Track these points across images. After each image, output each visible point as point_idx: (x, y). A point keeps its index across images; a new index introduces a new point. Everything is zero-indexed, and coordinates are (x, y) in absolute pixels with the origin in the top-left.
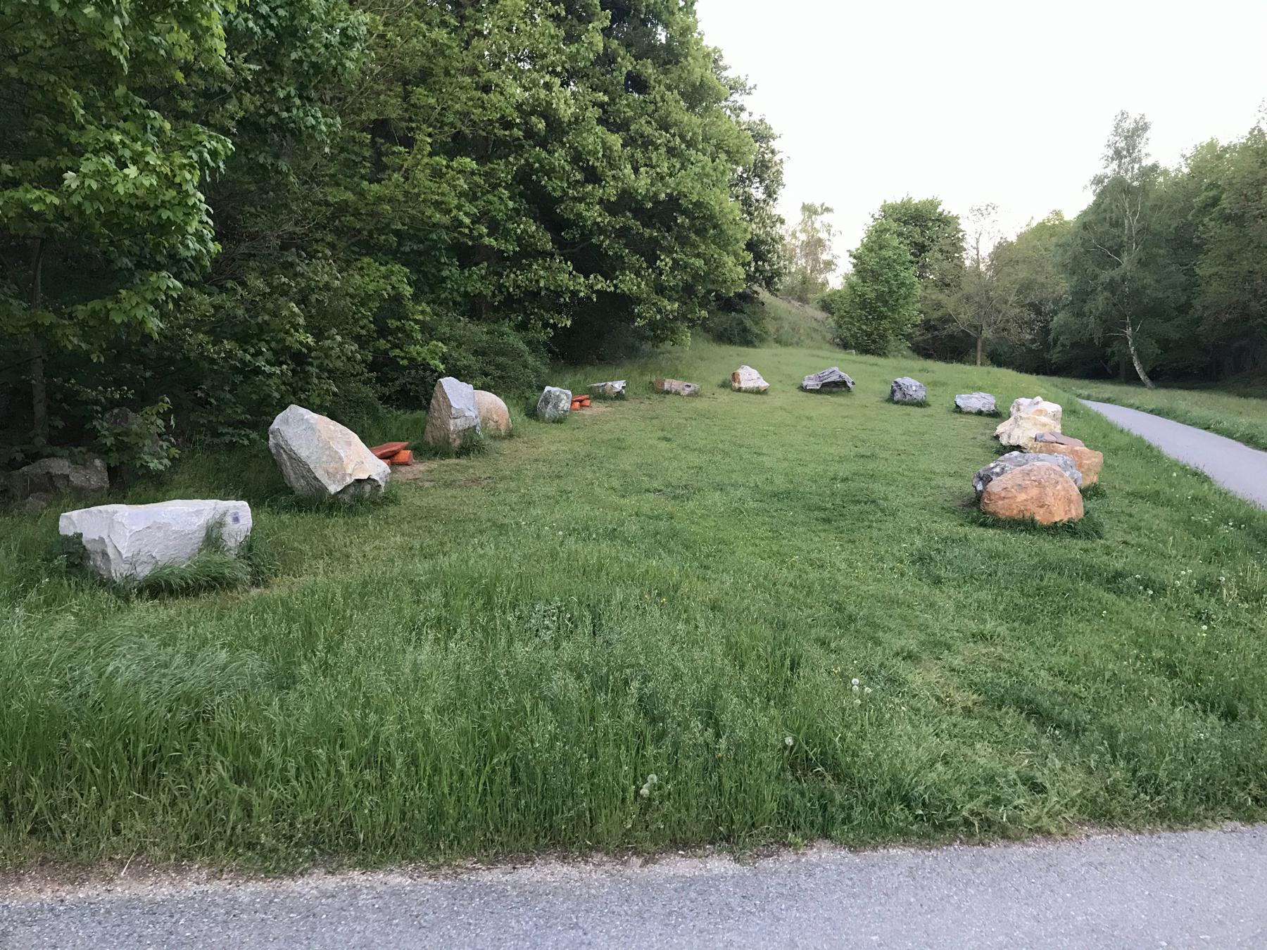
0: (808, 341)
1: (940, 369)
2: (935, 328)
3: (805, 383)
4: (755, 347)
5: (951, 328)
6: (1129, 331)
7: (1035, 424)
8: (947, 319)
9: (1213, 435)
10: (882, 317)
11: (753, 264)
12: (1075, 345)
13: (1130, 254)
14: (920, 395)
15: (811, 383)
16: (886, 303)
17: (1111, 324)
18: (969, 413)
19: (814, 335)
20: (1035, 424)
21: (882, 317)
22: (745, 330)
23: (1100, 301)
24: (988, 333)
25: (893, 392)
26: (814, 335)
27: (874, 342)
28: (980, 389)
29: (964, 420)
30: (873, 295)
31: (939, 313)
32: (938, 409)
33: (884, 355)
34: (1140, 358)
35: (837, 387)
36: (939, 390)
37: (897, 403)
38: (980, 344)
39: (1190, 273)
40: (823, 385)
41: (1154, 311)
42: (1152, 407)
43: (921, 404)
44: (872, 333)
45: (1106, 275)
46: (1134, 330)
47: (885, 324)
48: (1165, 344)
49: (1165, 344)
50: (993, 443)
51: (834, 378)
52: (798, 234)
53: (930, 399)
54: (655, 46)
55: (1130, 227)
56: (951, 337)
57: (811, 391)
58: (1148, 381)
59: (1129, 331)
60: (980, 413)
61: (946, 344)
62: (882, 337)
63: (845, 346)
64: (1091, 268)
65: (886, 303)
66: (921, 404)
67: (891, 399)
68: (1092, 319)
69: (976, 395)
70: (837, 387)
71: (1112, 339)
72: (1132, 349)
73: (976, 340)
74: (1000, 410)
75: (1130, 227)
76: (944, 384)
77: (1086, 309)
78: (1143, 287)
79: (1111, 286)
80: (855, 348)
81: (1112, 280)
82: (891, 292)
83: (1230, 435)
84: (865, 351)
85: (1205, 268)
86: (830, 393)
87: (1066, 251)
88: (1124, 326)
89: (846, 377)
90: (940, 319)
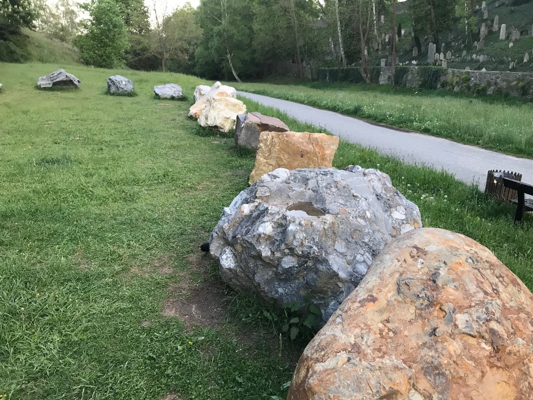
0: (63, 60)
1: (143, 74)
2: (139, 54)
3: (39, 83)
4: (21, 63)
5: (147, 55)
6: (229, 56)
7: (227, 105)
8: (144, 49)
9: (299, 104)
10: (106, 45)
11: (10, 7)
12: (207, 63)
13: (225, 19)
14: (129, 87)
15: (44, 82)
16: (107, 37)
17: (221, 52)
18: (165, 99)
19: (66, 57)
20: (227, 105)
21: (106, 45)
22: (12, 52)
23: (215, 42)
24: (167, 56)
25: (109, 86)
26: (66, 57)
27: (104, 60)
28: (168, 82)
29: (163, 104)
30: (99, 32)
31: (140, 47)
32: (143, 97)
33: (112, 68)
34: (234, 67)
35: (65, 85)
36: (144, 85)
37: (113, 94)
38: (163, 62)
39: (250, 28)
40: (54, 84)
41: (238, 47)
42: (253, 90)
43: (131, 94)
44: (102, 56)
45: (216, 29)
46: (231, 55)
47: (109, 49)
48: (243, 61)
49: (243, 61)
50: (190, 123)
51: (61, 78)
52: (60, 7)
53: (137, 91)
54: (92, 36)
55: (224, 5)
56: (148, 58)
57: (45, 89)
58: (239, 80)
59: (229, 56)
60: (173, 98)
61: (145, 61)
62: (108, 57)
63: (87, 63)
64: (210, 25)
65: (107, 37)
66: (131, 94)
67: (108, 92)
68: (213, 50)
69: (168, 85)
70: (65, 85)
71: (223, 60)
72: (231, 65)
73: (161, 60)
74: (186, 95)
75: (224, 5)
76: (146, 81)
77: (210, 46)
78: (233, 34)
79: (219, 34)
80: (93, 65)
81: (219, 31)
82: (109, 30)
83: (302, 102)
84: (100, 65)
85: (256, 26)
86: (61, 90)
87: (197, 17)
88: (226, 53)
89: (72, 77)
90: (141, 49)
